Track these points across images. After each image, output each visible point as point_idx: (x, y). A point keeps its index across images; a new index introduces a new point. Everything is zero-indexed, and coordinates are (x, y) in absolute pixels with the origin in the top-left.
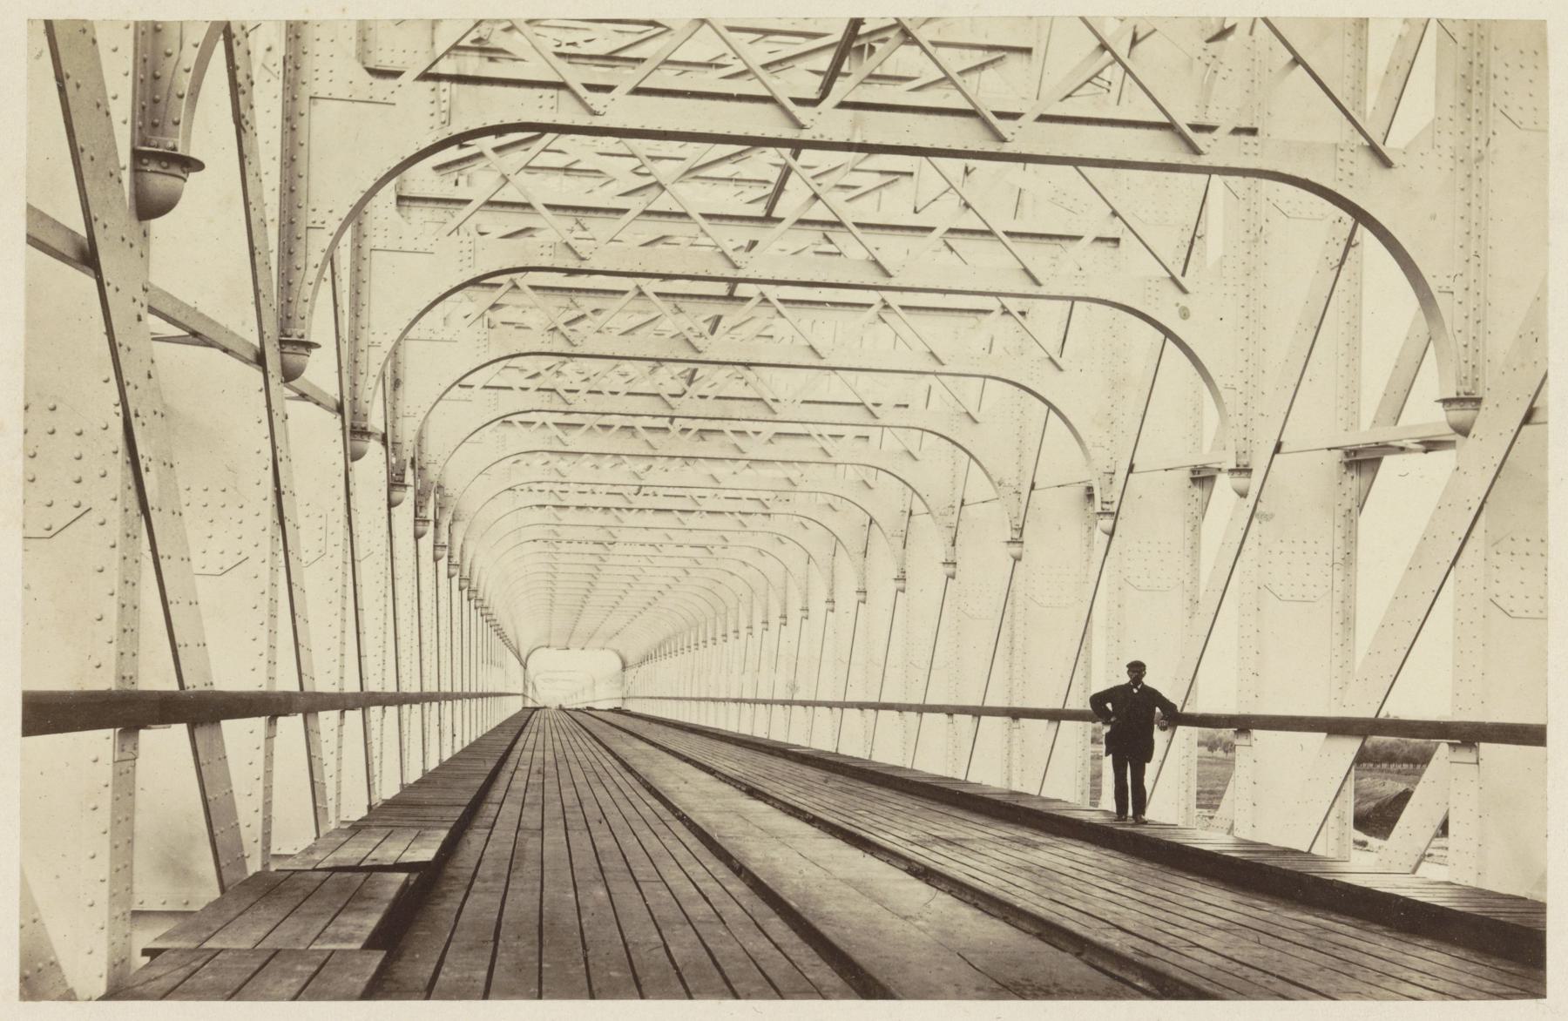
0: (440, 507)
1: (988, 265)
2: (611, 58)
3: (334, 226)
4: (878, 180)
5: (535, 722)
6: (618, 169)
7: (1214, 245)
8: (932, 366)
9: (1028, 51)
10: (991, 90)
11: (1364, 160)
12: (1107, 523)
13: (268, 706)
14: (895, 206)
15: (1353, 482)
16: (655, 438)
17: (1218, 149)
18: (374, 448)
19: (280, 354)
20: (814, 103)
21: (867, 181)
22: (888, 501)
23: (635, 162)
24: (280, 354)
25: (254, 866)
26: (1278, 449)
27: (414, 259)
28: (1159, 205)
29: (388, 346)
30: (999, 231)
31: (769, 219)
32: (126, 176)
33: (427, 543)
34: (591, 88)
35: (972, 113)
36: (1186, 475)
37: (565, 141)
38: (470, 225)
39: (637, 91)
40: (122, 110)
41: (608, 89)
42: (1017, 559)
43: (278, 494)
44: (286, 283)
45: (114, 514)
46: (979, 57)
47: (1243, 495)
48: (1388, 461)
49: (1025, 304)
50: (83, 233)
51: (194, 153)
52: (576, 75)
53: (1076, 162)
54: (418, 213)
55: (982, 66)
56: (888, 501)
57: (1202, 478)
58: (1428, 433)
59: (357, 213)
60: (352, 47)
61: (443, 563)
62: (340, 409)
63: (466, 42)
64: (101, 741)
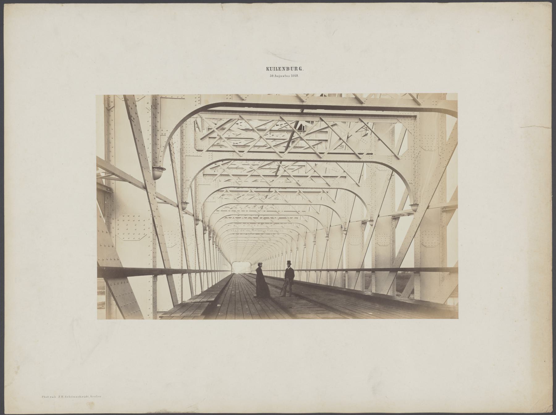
0: (213, 234)
1: (320, 183)
2: (245, 146)
3: (191, 180)
4: (298, 167)
5: (234, 276)
6: (247, 167)
7: (365, 177)
8: (309, 203)
9: (327, 140)
10: (320, 148)
11: (394, 158)
12: (345, 232)
13: (182, 272)
14: (302, 172)
15: (394, 222)
16: (255, 220)
17: (364, 158)
18: (200, 223)
19: (182, 205)
20: (283, 152)
21: (296, 168)
22: (302, 230)
23: (249, 166)
24: (182, 205)
25: (180, 302)
26: (378, 216)
27: (206, 186)
28: (354, 169)
29: (202, 203)
30: (321, 176)
31: (276, 176)
32: (151, 172)
33: (211, 241)
34: (240, 152)
35: (315, 153)
36: (361, 222)
37: (236, 162)
38: (218, 179)
39: (249, 152)
40: (150, 160)
41: (243, 152)
42: (328, 240)
43: (182, 232)
44: (182, 191)
45: (151, 235)
46: (318, 142)
47: (372, 225)
48: (401, 218)
49: (328, 190)
50: (144, 183)
51: (164, 167)
52: (237, 149)
53: (336, 161)
54: (208, 177)
55: (318, 144)
56: (302, 230)
57: (364, 223)
58: (408, 211)
59: (195, 178)
60: (193, 146)
61: (215, 245)
62: (193, 216)
63: (215, 144)
64: (150, 278)
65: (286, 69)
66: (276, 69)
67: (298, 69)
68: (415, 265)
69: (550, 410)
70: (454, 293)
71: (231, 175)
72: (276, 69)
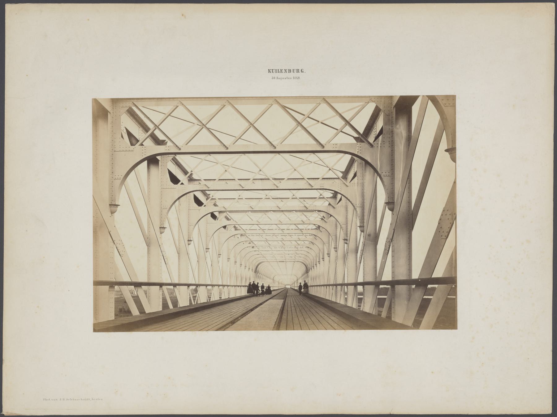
65: (288, 71)
66: (277, 71)
67: (300, 71)
68: (393, 278)
71: (271, 179)
72: (277, 71)
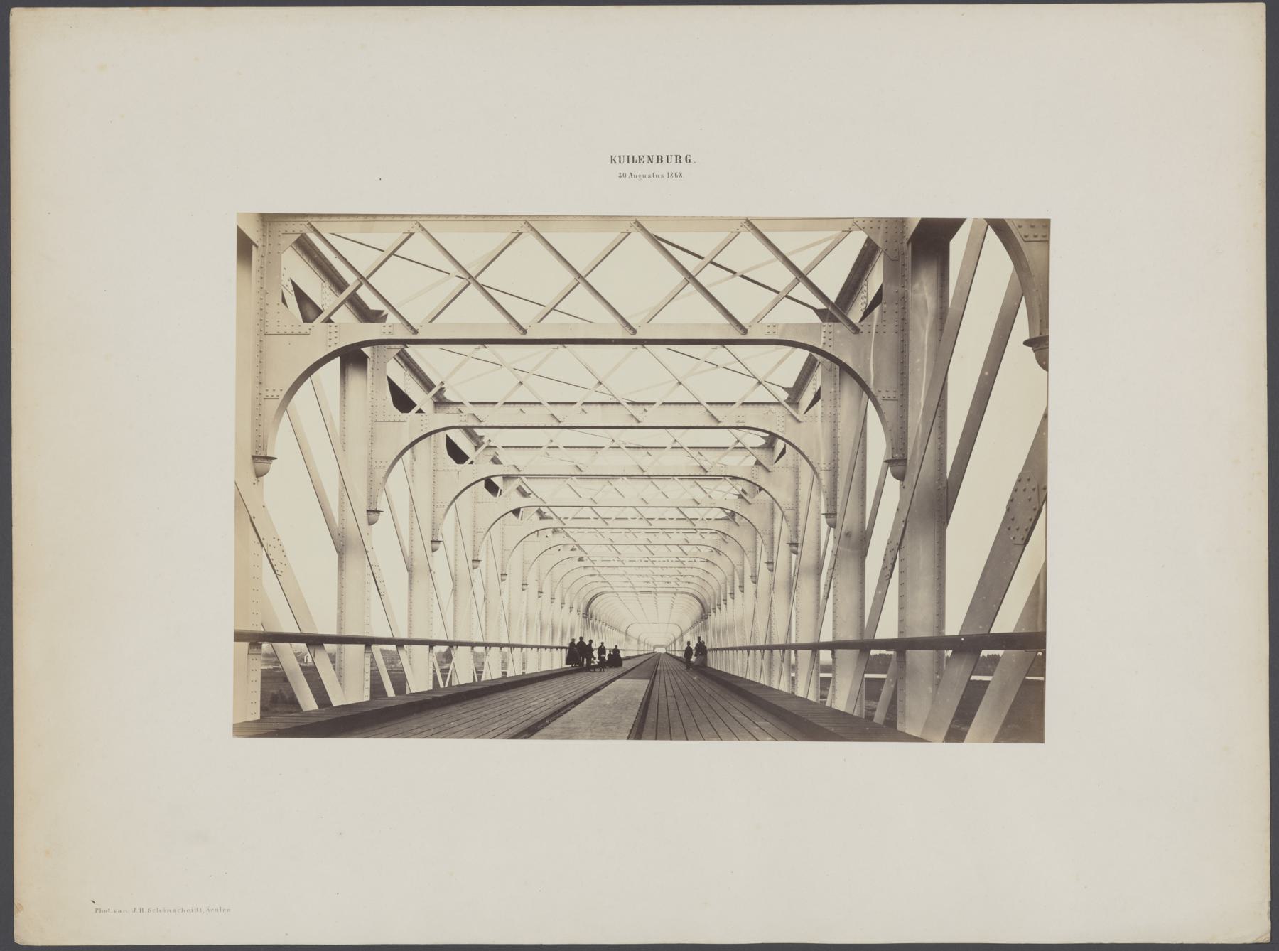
65: (655, 159)
66: (632, 160)
67: (683, 159)
68: (900, 632)
69: (1266, 938)
70: (981, 739)
71: (545, 403)
72: (632, 160)
